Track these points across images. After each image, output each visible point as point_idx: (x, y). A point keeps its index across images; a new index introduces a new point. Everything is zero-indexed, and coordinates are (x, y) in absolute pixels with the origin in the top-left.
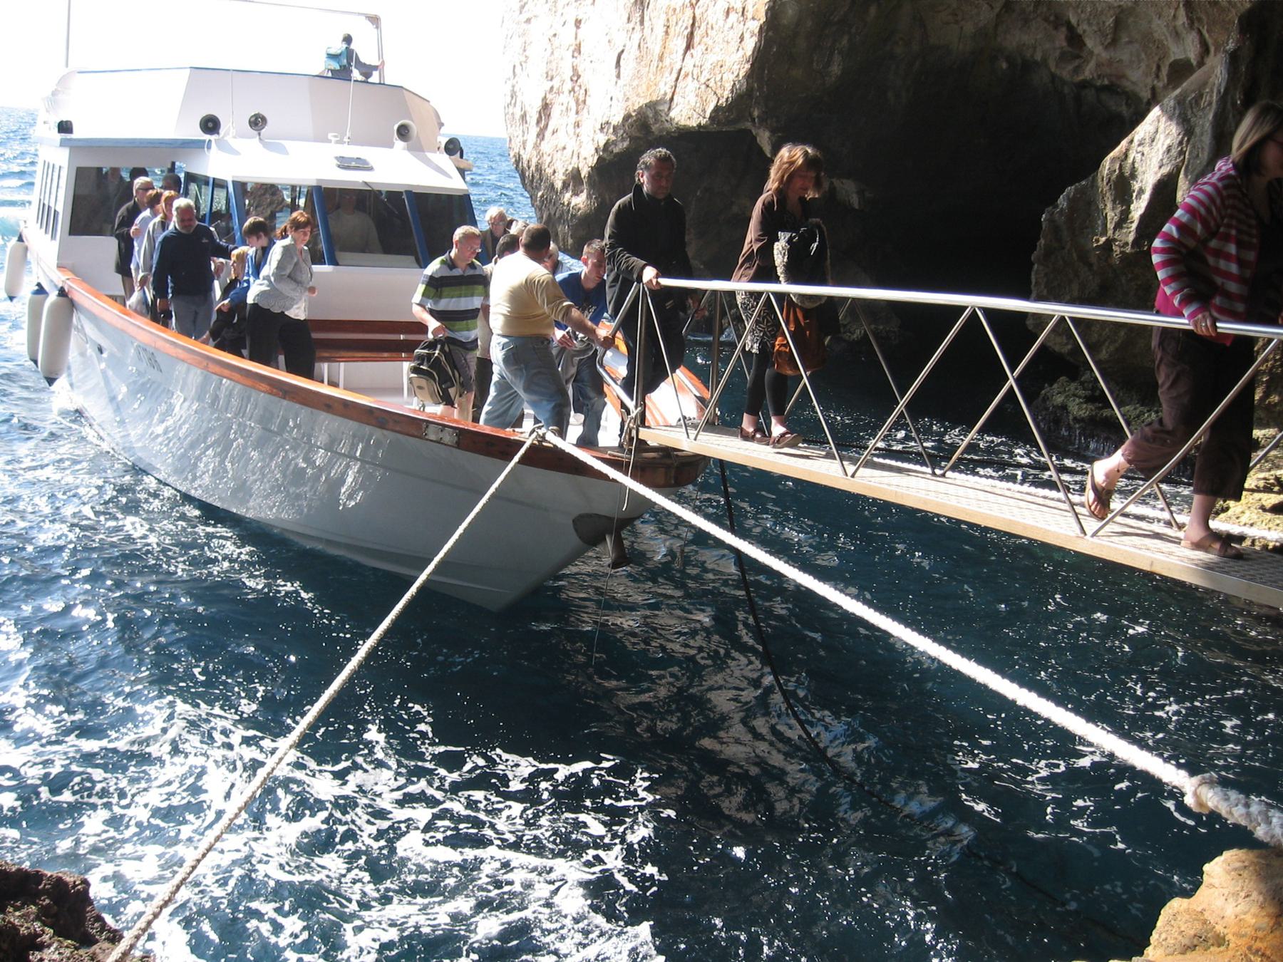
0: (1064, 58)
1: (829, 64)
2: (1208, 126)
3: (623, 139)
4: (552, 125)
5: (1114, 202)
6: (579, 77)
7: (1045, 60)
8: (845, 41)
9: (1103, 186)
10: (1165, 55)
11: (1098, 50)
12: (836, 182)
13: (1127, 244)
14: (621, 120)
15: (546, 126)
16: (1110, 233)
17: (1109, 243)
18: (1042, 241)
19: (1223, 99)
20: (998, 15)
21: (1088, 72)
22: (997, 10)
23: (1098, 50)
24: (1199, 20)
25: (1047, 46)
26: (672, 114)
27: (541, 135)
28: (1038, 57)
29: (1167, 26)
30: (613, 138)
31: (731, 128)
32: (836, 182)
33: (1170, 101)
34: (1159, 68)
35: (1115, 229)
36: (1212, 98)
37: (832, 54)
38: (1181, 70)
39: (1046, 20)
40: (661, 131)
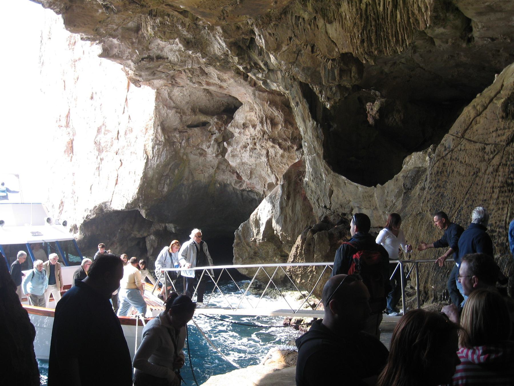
0: (236, 182)
1: (163, 188)
2: (278, 205)
3: (93, 214)
4: (65, 209)
5: (255, 227)
6: (75, 192)
7: (231, 184)
8: (168, 181)
9: (251, 223)
10: (266, 181)
11: (246, 180)
12: (167, 225)
13: (260, 240)
14: (93, 208)
15: (62, 210)
16: (255, 237)
17: (255, 239)
18: (235, 241)
19: (281, 197)
20: (215, 171)
21: (244, 187)
22: (215, 169)
23: (246, 180)
24: (274, 171)
25: (231, 179)
26: (111, 206)
27: (60, 212)
28: (228, 182)
29: (266, 173)
30: (90, 214)
31: (133, 210)
32: (167, 225)
33: (268, 198)
34: (265, 185)
35: (256, 235)
36: (278, 197)
37: (164, 185)
38: (271, 186)
39: (230, 171)
40: (107, 211)
